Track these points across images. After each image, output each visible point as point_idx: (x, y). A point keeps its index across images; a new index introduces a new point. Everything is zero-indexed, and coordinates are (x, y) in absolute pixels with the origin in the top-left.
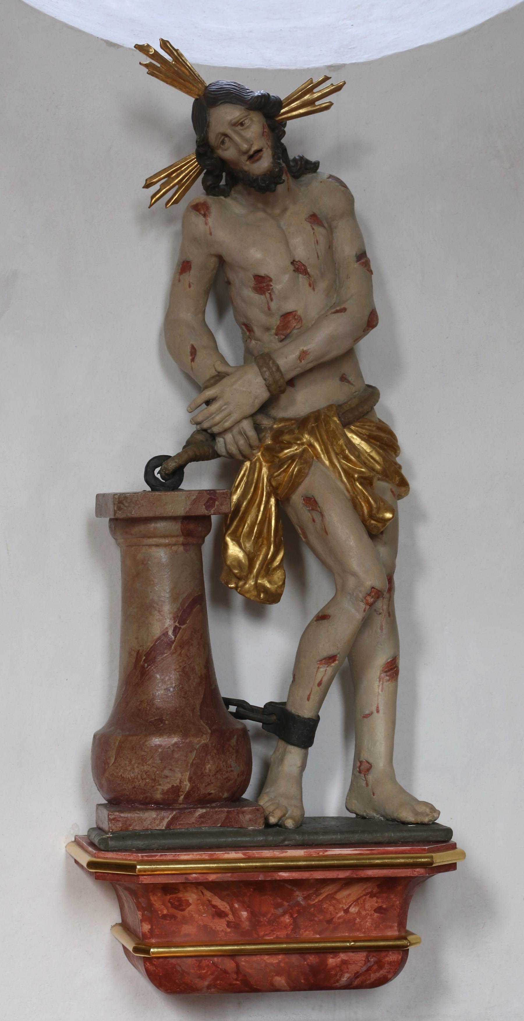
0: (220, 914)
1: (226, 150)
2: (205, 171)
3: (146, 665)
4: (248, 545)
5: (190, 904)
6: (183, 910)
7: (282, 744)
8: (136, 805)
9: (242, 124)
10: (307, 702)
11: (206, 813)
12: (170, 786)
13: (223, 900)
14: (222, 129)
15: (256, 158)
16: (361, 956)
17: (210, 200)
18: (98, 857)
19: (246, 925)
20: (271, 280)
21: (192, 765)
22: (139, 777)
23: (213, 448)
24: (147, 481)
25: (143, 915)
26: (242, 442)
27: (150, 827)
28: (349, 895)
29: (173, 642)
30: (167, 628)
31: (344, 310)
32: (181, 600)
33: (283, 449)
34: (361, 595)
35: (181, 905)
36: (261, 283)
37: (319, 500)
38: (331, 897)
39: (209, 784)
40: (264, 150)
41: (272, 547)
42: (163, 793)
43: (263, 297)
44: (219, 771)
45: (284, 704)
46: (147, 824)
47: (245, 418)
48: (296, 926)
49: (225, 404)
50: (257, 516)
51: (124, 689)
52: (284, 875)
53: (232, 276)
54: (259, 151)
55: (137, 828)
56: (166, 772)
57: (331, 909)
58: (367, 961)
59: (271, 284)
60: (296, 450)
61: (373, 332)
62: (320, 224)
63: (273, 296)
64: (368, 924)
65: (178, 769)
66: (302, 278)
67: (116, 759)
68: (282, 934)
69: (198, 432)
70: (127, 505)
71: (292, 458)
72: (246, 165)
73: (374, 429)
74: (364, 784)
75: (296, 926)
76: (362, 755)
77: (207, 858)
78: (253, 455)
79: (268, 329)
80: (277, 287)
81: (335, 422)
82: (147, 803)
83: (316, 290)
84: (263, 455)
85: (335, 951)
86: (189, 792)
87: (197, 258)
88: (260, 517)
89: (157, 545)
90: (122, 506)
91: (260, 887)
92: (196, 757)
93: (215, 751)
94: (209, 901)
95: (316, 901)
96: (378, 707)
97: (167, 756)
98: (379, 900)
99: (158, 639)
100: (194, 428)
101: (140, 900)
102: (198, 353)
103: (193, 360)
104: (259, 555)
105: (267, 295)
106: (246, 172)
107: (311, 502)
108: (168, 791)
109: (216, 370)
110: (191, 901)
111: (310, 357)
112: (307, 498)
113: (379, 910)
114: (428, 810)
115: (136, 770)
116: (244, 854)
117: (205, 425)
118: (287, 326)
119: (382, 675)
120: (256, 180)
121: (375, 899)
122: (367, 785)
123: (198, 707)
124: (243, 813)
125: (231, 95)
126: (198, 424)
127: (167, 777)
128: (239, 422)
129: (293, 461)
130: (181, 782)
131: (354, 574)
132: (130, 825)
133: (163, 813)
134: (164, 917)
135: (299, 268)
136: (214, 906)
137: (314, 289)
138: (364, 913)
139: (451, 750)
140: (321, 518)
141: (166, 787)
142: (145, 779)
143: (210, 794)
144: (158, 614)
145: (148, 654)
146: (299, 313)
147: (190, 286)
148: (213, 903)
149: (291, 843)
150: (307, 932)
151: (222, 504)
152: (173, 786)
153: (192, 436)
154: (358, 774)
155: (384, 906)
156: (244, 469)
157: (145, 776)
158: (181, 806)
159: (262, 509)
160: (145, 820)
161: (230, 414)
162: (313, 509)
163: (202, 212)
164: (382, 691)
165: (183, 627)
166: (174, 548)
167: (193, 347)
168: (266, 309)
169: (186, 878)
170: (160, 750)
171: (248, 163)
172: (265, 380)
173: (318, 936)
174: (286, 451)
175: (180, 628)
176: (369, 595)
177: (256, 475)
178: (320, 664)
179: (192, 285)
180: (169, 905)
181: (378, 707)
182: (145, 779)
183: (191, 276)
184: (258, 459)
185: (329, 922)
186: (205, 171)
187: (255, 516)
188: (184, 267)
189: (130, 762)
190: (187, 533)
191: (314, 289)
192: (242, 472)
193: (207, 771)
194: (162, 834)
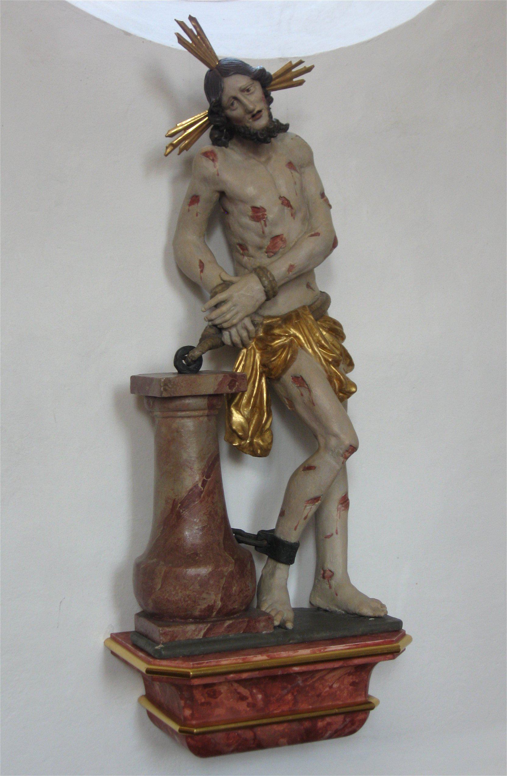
0: (242, 698)
1: (234, 110)
2: (212, 126)
3: (181, 511)
4: (246, 413)
5: (222, 693)
6: (216, 698)
7: (272, 562)
8: (177, 619)
9: (248, 90)
10: (294, 531)
11: (232, 623)
12: (206, 605)
13: (245, 688)
14: (233, 94)
15: (258, 117)
16: (340, 718)
17: (216, 149)
18: (154, 665)
19: (261, 704)
20: (265, 210)
21: (223, 588)
22: (182, 599)
23: (221, 339)
24: (176, 366)
25: (185, 704)
26: (245, 334)
27: (191, 637)
28: (334, 676)
29: (202, 492)
30: (197, 482)
31: (317, 234)
32: (207, 459)
33: (274, 340)
34: (341, 452)
35: (214, 695)
36: (257, 213)
37: (306, 379)
38: (322, 678)
39: (234, 602)
40: (263, 111)
41: (266, 414)
42: (201, 611)
43: (258, 224)
44: (241, 591)
45: (273, 531)
46: (188, 635)
47: (247, 316)
48: (295, 701)
49: (234, 306)
50: (253, 391)
51: (162, 528)
52: (296, 669)
53: (230, 207)
54: (260, 112)
55: (181, 639)
56: (204, 595)
57: (321, 686)
58: (344, 720)
59: (266, 213)
60: (285, 340)
61: (335, 251)
62: (295, 169)
63: (267, 223)
64: (345, 694)
65: (213, 593)
66: (287, 210)
67: (162, 585)
68: (286, 708)
69: (210, 327)
70: (170, 386)
71: (283, 347)
72: (248, 122)
73: (332, 323)
74: (327, 586)
75: (295, 701)
76: (326, 565)
77: (241, 661)
78: (249, 345)
79: (260, 248)
80: (270, 216)
81: (311, 319)
82: (186, 617)
83: (296, 219)
84: (256, 344)
85: (323, 717)
86: (220, 608)
87: (206, 193)
88: (255, 392)
89: (189, 417)
90: (167, 388)
91: (274, 678)
92: (226, 581)
93: (238, 576)
94: (236, 690)
95: (311, 682)
96: (337, 530)
97: (204, 583)
98: (354, 677)
99: (191, 490)
100: (206, 324)
101: (184, 693)
102: (205, 266)
103: (202, 271)
104: (253, 420)
105: (263, 222)
106: (247, 127)
107: (299, 380)
108: (205, 609)
109: (222, 279)
110: (222, 691)
111: (295, 270)
112: (295, 377)
113: (353, 684)
114: (379, 606)
115: (180, 594)
116: (268, 656)
117: (217, 322)
118: (275, 245)
119: (339, 506)
120: (256, 134)
121: (351, 677)
122: (330, 587)
123: (221, 541)
124: (259, 621)
125: (239, 68)
126: (210, 321)
127: (204, 599)
128: (242, 319)
129: (285, 349)
130: (215, 602)
131: (336, 436)
132: (176, 637)
133: (201, 626)
134: (202, 704)
135: (286, 202)
136: (239, 693)
137: (294, 218)
138: (342, 687)
139: (382, 555)
140: (308, 393)
141: (204, 606)
142: (187, 601)
143: (234, 609)
144: (190, 471)
145: (182, 503)
146: (285, 236)
147: (197, 215)
148: (239, 690)
149: (295, 641)
150: (303, 705)
151: (240, 384)
152: (209, 606)
153: (205, 330)
154: (322, 579)
155: (357, 681)
156: (242, 354)
157: (187, 599)
158: (213, 620)
159: (256, 385)
160: (187, 632)
161: (237, 313)
162: (300, 386)
163: (211, 158)
164: (339, 518)
165: (209, 480)
166: (201, 419)
167: (201, 262)
168: (261, 233)
169: (226, 678)
170: (199, 578)
171: (251, 120)
172: (264, 287)
173: (310, 707)
174: (277, 342)
175: (206, 481)
176: (347, 451)
177: (252, 360)
178: (307, 503)
179: (199, 214)
180: (206, 695)
181: (337, 530)
182: (187, 601)
183: (197, 208)
184: (253, 348)
185: (319, 696)
186: (212, 126)
187: (251, 390)
188: (194, 199)
189: (175, 588)
190: (211, 407)
191: (294, 218)
192: (240, 358)
193: (233, 592)
194: (199, 642)
